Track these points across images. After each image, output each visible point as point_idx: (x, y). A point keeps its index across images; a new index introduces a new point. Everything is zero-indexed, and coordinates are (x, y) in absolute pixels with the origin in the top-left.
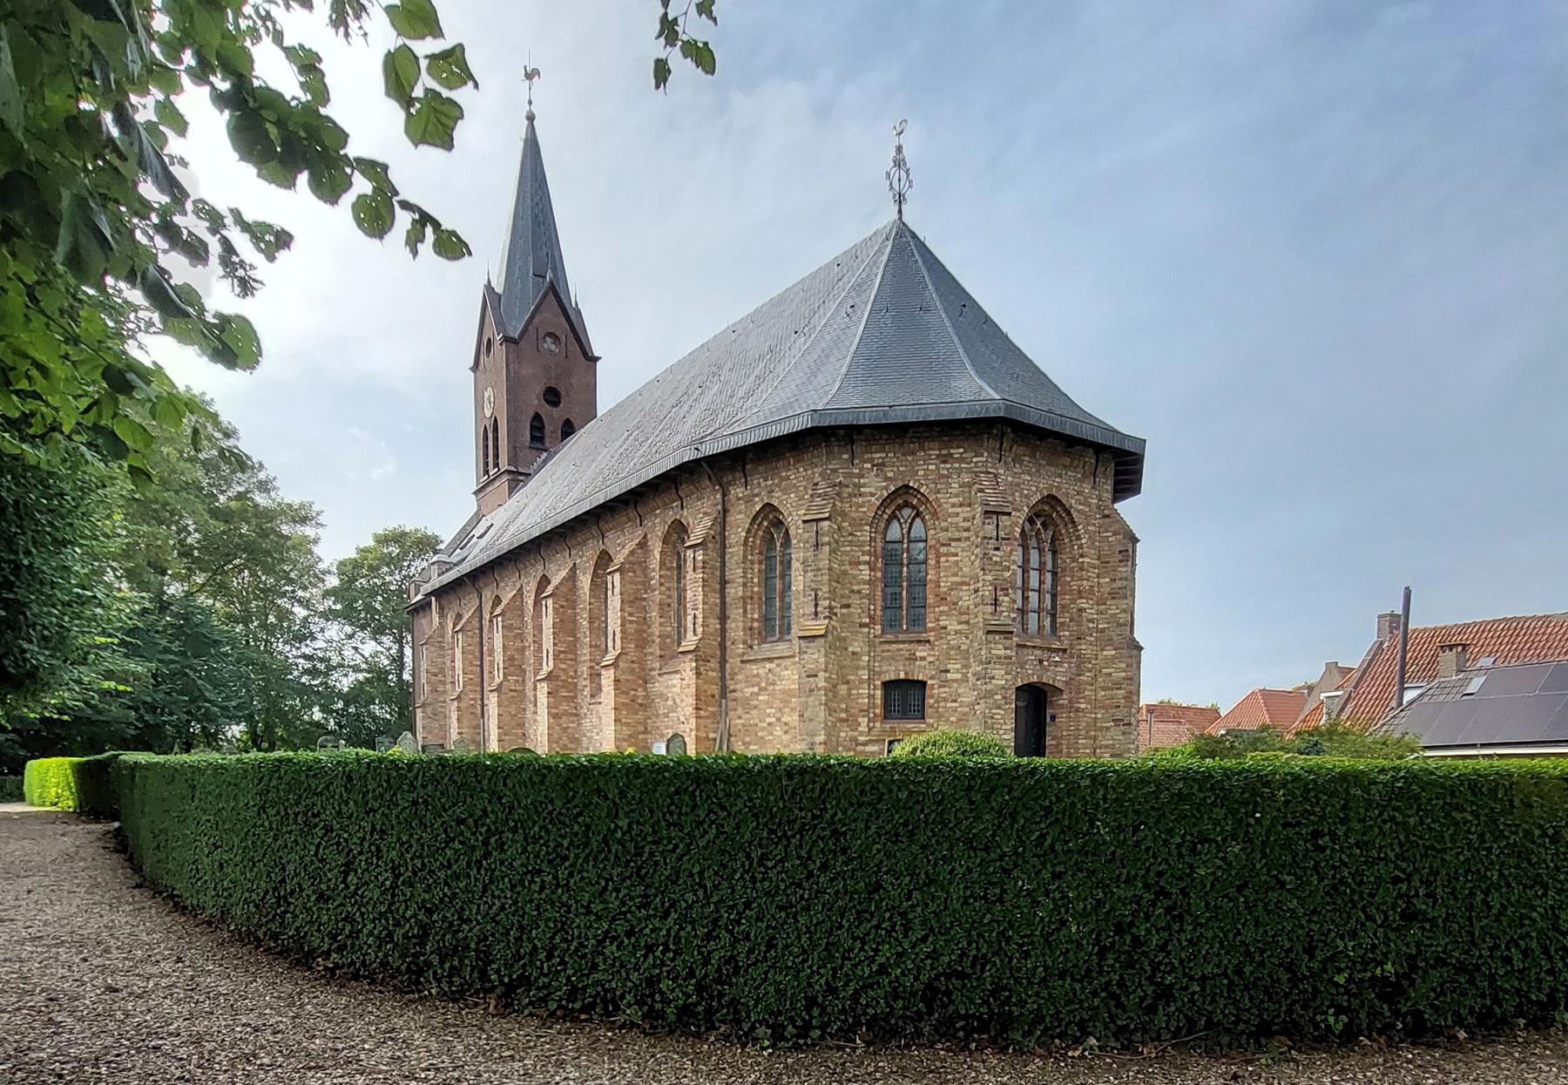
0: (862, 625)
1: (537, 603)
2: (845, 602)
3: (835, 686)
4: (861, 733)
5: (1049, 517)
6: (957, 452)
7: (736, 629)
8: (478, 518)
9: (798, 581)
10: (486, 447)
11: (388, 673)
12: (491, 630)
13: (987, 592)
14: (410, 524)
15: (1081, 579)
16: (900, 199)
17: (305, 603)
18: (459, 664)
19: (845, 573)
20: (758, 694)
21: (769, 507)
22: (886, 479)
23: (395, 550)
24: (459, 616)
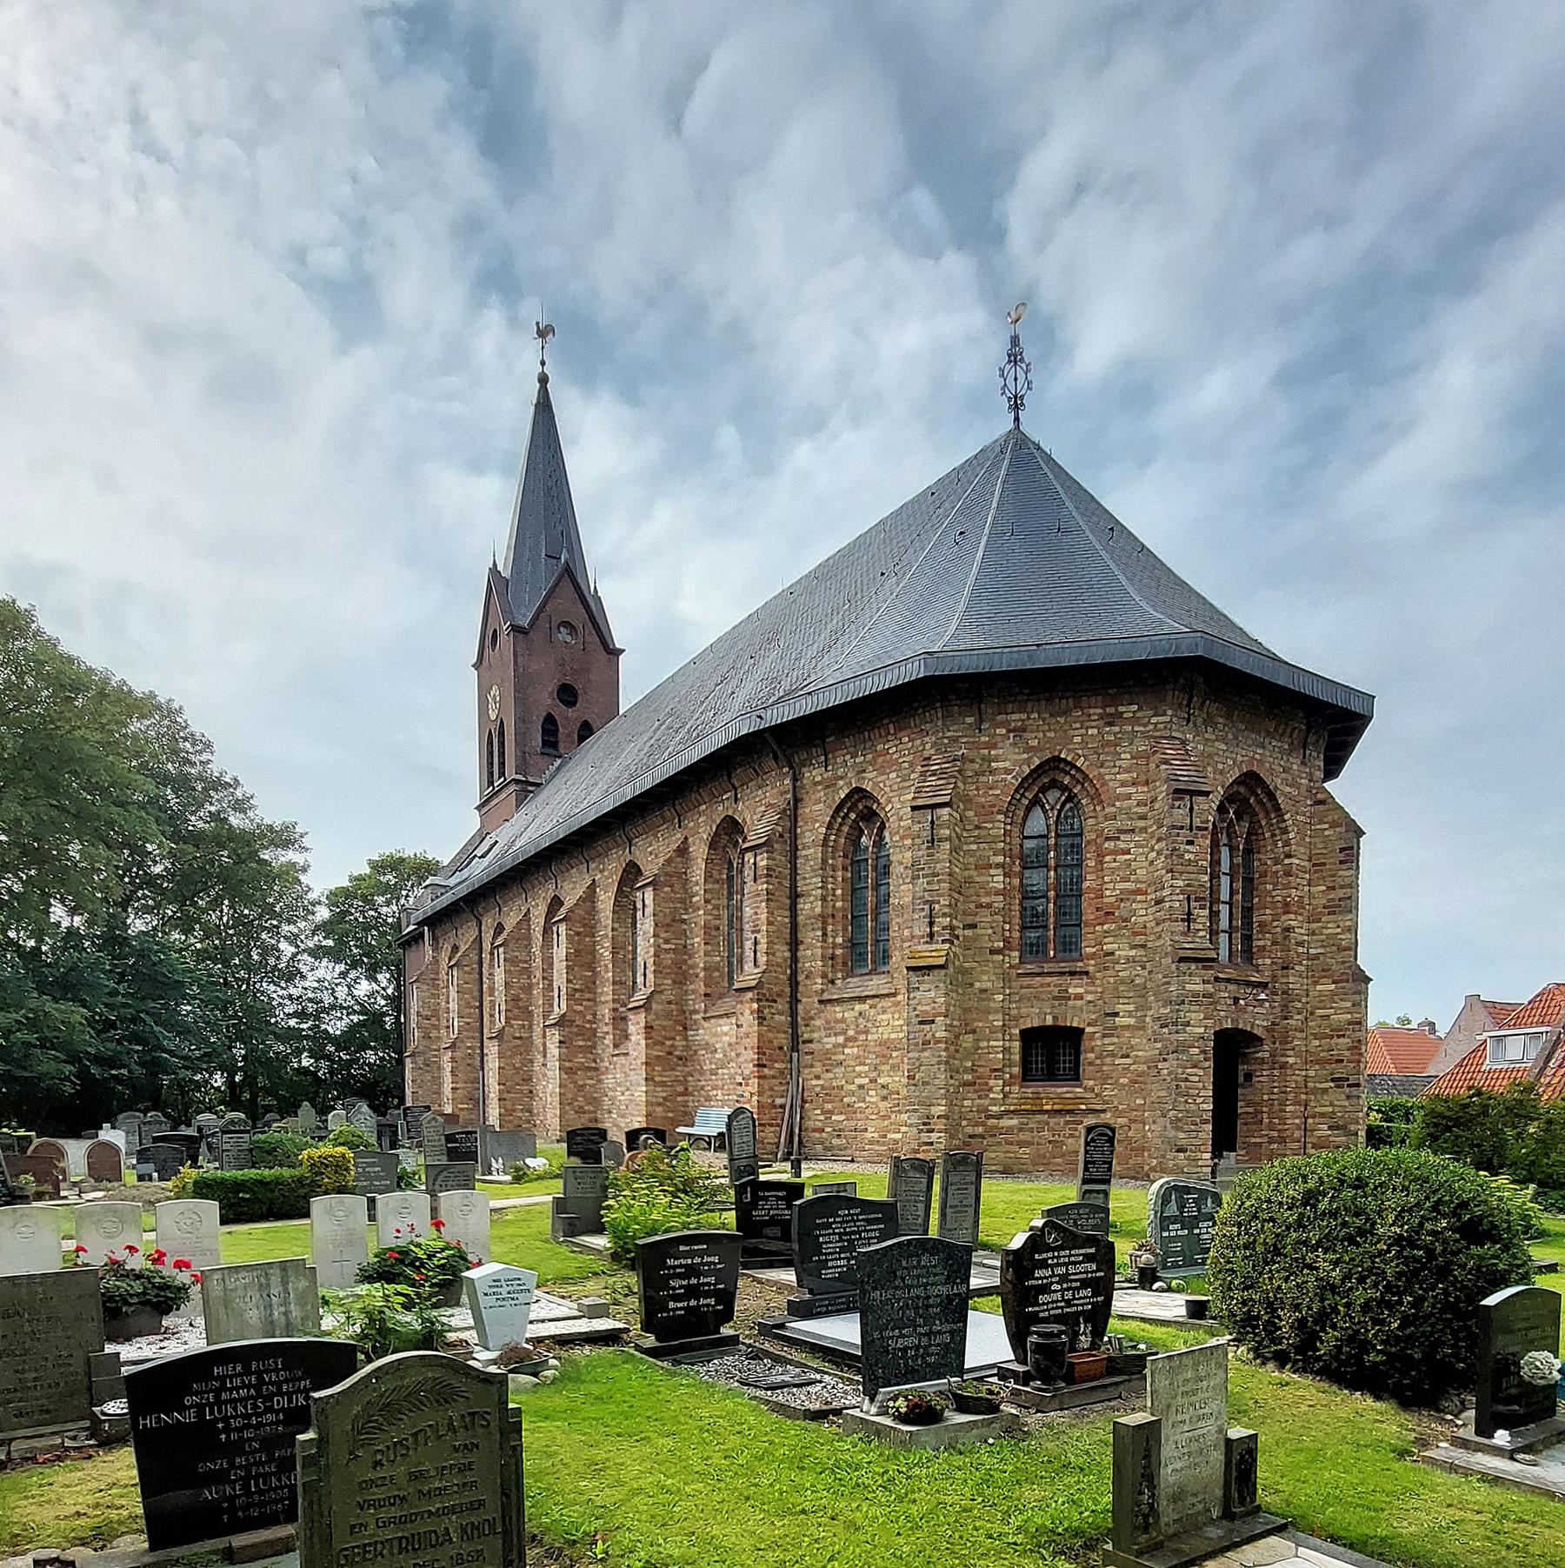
0: (992, 952)
1: (547, 931)
2: (969, 920)
3: (957, 1037)
4: (994, 1102)
5: (1249, 800)
6: (1128, 710)
7: (812, 956)
8: (481, 836)
9: (902, 891)
10: (491, 754)
11: (385, 1014)
12: (491, 966)
13: (1177, 903)
14: (409, 850)
15: (1287, 887)
16: (1016, 404)
17: (293, 939)
18: (453, 1006)
19: (969, 881)
20: (844, 1046)
21: (858, 794)
22: (1028, 749)
23: (390, 878)
24: (455, 948)
